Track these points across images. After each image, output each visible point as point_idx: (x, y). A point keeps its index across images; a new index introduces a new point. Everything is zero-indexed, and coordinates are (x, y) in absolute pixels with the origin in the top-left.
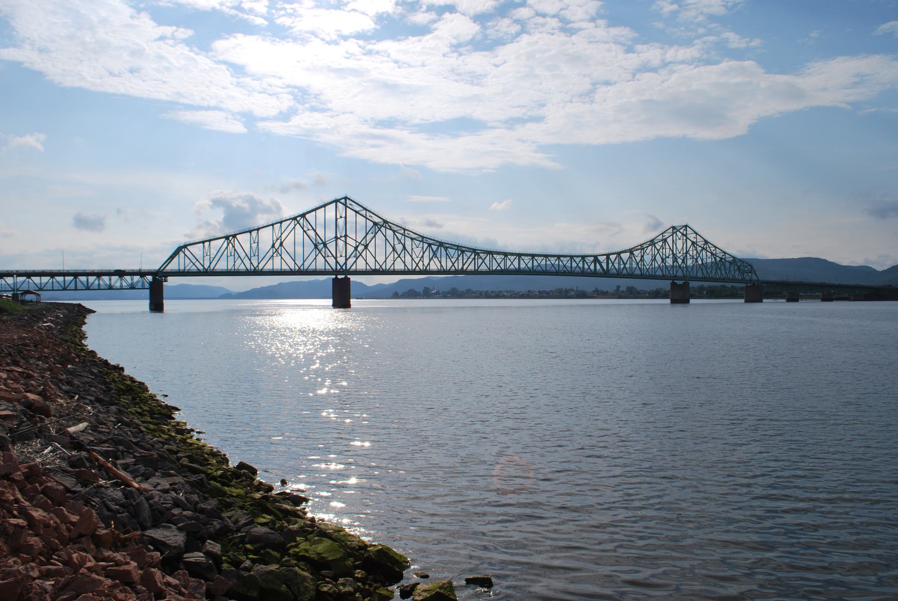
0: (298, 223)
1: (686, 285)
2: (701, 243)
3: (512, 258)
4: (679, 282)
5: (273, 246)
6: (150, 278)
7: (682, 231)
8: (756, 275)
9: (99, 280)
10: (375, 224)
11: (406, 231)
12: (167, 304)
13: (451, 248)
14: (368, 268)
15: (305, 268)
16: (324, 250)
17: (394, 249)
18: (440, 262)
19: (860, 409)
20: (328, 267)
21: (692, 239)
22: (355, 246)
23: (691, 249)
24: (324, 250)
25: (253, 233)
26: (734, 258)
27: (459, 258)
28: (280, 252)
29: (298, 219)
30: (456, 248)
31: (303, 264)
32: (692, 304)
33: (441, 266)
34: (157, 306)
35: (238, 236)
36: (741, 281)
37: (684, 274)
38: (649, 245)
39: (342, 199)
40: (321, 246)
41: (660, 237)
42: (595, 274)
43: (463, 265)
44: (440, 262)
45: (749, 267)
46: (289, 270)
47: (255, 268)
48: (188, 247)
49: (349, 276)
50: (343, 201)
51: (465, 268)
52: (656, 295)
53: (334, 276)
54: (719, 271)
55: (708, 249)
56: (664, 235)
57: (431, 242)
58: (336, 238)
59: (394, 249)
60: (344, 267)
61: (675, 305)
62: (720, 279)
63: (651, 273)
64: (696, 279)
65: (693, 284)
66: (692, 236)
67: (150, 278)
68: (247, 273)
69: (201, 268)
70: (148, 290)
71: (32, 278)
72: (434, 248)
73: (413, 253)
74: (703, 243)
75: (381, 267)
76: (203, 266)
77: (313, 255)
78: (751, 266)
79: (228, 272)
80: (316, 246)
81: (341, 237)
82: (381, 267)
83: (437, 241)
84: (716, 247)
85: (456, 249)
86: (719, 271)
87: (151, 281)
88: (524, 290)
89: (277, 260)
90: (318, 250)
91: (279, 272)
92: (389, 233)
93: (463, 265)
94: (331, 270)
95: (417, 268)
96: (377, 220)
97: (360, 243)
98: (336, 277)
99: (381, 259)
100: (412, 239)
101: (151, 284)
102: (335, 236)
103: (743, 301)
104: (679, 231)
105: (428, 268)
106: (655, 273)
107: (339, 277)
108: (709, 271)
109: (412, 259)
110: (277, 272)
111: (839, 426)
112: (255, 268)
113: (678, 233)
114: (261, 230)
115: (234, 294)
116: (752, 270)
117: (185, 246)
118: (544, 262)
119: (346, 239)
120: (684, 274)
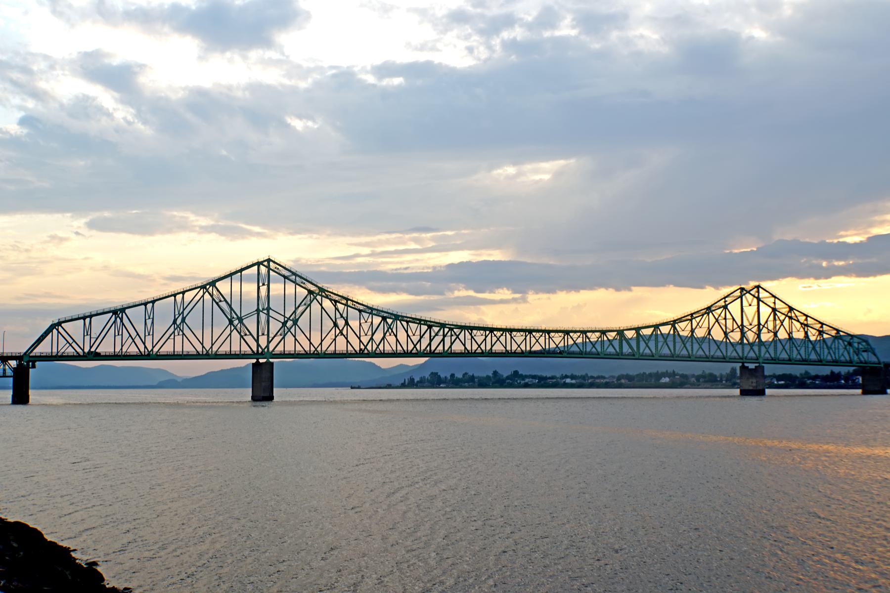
0: (207, 291)
1: (759, 370)
3: (538, 335)
4: (752, 366)
5: (175, 322)
6: (13, 363)
7: (752, 292)
8: (875, 355)
9: (4, 366)
10: (310, 292)
11: (349, 302)
12: (34, 395)
13: (414, 323)
14: (350, 348)
15: (324, 349)
16: (239, 325)
17: (336, 325)
18: (144, 343)
20: (299, 348)
22: (283, 321)
24: (239, 325)
25: (773, 304)
26: (838, 331)
28: (181, 328)
29: (208, 287)
30: (418, 322)
31: (321, 344)
32: (30, 404)
33: (145, 347)
34: (21, 397)
35: (127, 311)
36: (850, 363)
38: (705, 313)
39: (265, 261)
40: (236, 322)
41: (722, 303)
42: (619, 356)
43: (91, 347)
44: (144, 343)
45: (864, 344)
46: (195, 353)
47: (207, 352)
48: (63, 325)
49: (271, 360)
50: (266, 263)
51: (215, 349)
52: (711, 381)
53: (254, 361)
56: (727, 299)
57: (385, 315)
58: (258, 311)
59: (336, 325)
60: (319, 349)
61: (258, 403)
64: (775, 361)
65: (769, 370)
67: (13, 363)
68: (198, 356)
69: (200, 349)
70: (11, 379)
71: (9, 361)
72: (389, 321)
74: (788, 309)
75: (479, 346)
76: (83, 350)
77: (332, 335)
78: (866, 341)
79: (115, 356)
80: (231, 322)
81: (263, 309)
83: (392, 314)
84: (807, 316)
85: (418, 324)
87: (15, 366)
89: (391, 339)
90: (234, 326)
91: (293, 354)
92: (327, 303)
93: (91, 347)
96: (313, 288)
97: (289, 319)
98: (258, 361)
99: (316, 341)
100: (360, 311)
101: (15, 370)
102: (256, 308)
103: (737, 392)
104: (749, 292)
105: (381, 347)
107: (261, 361)
109: (408, 336)
110: (290, 354)
111: (791, 536)
112: (207, 352)
113: (748, 295)
114: (157, 302)
115: (179, 380)
116: (869, 349)
117: (59, 324)
118: (580, 340)
119: (268, 312)
120: (672, 353)
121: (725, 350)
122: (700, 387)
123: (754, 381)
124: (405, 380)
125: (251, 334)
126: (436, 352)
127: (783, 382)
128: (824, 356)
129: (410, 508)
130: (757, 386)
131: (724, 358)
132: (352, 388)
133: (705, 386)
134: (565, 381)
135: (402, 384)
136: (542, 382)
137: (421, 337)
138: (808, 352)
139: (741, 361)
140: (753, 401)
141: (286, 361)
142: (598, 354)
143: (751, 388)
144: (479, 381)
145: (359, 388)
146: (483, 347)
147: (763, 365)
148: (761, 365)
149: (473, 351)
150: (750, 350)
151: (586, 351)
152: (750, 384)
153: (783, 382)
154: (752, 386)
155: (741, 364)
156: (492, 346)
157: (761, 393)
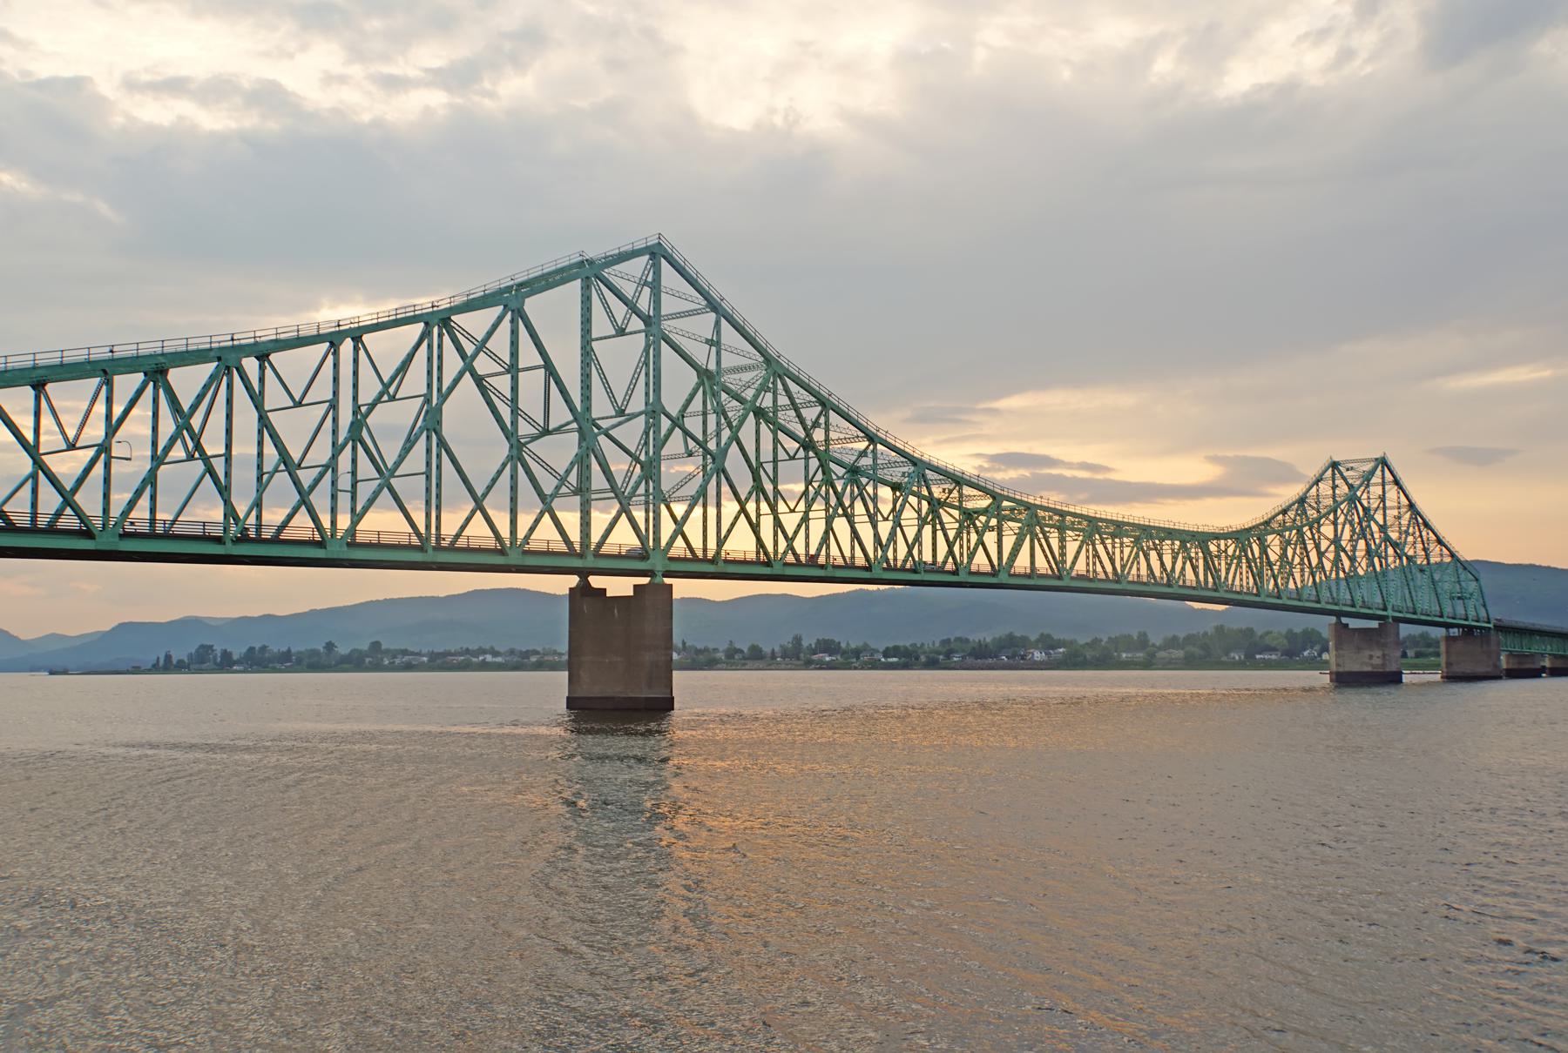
1: (653, 600)
2: (747, 380)
4: (618, 587)
19: (908, 1042)
21: (700, 353)
23: (697, 404)
27: (771, 487)
32: (1407, 685)
37: (760, 543)
54: (841, 525)
55: (787, 418)
62: (850, 566)
63: (697, 544)
66: (694, 330)
73: (47, 421)
75: (68, 499)
82: (68, 499)
86: (841, 525)
88: (931, 639)
94: (563, 547)
95: (680, 542)
106: (721, 543)
108: (790, 522)
120: (760, 543)
121: (507, 518)
122: (747, 667)
123: (1378, 653)
124: (158, 658)
125: (354, 498)
126: (605, 549)
127: (895, 660)
128: (1087, 551)
129: (343, 1030)
130: (1383, 665)
131: (768, 564)
132: (52, 673)
133: (755, 666)
134: (485, 659)
135: (154, 666)
136: (439, 661)
137: (151, 480)
138: (1039, 540)
139: (577, 563)
140: (1361, 701)
141: (868, 591)
142: (87, 534)
143: (1369, 669)
144: (296, 659)
145: (65, 672)
146: (799, 545)
147: (667, 581)
148: (658, 580)
149: (899, 564)
150: (473, 513)
151: (439, 537)
152: (1366, 660)
153: (895, 660)
154: (1372, 665)
155: (573, 580)
156: (357, 518)
157: (1394, 679)
